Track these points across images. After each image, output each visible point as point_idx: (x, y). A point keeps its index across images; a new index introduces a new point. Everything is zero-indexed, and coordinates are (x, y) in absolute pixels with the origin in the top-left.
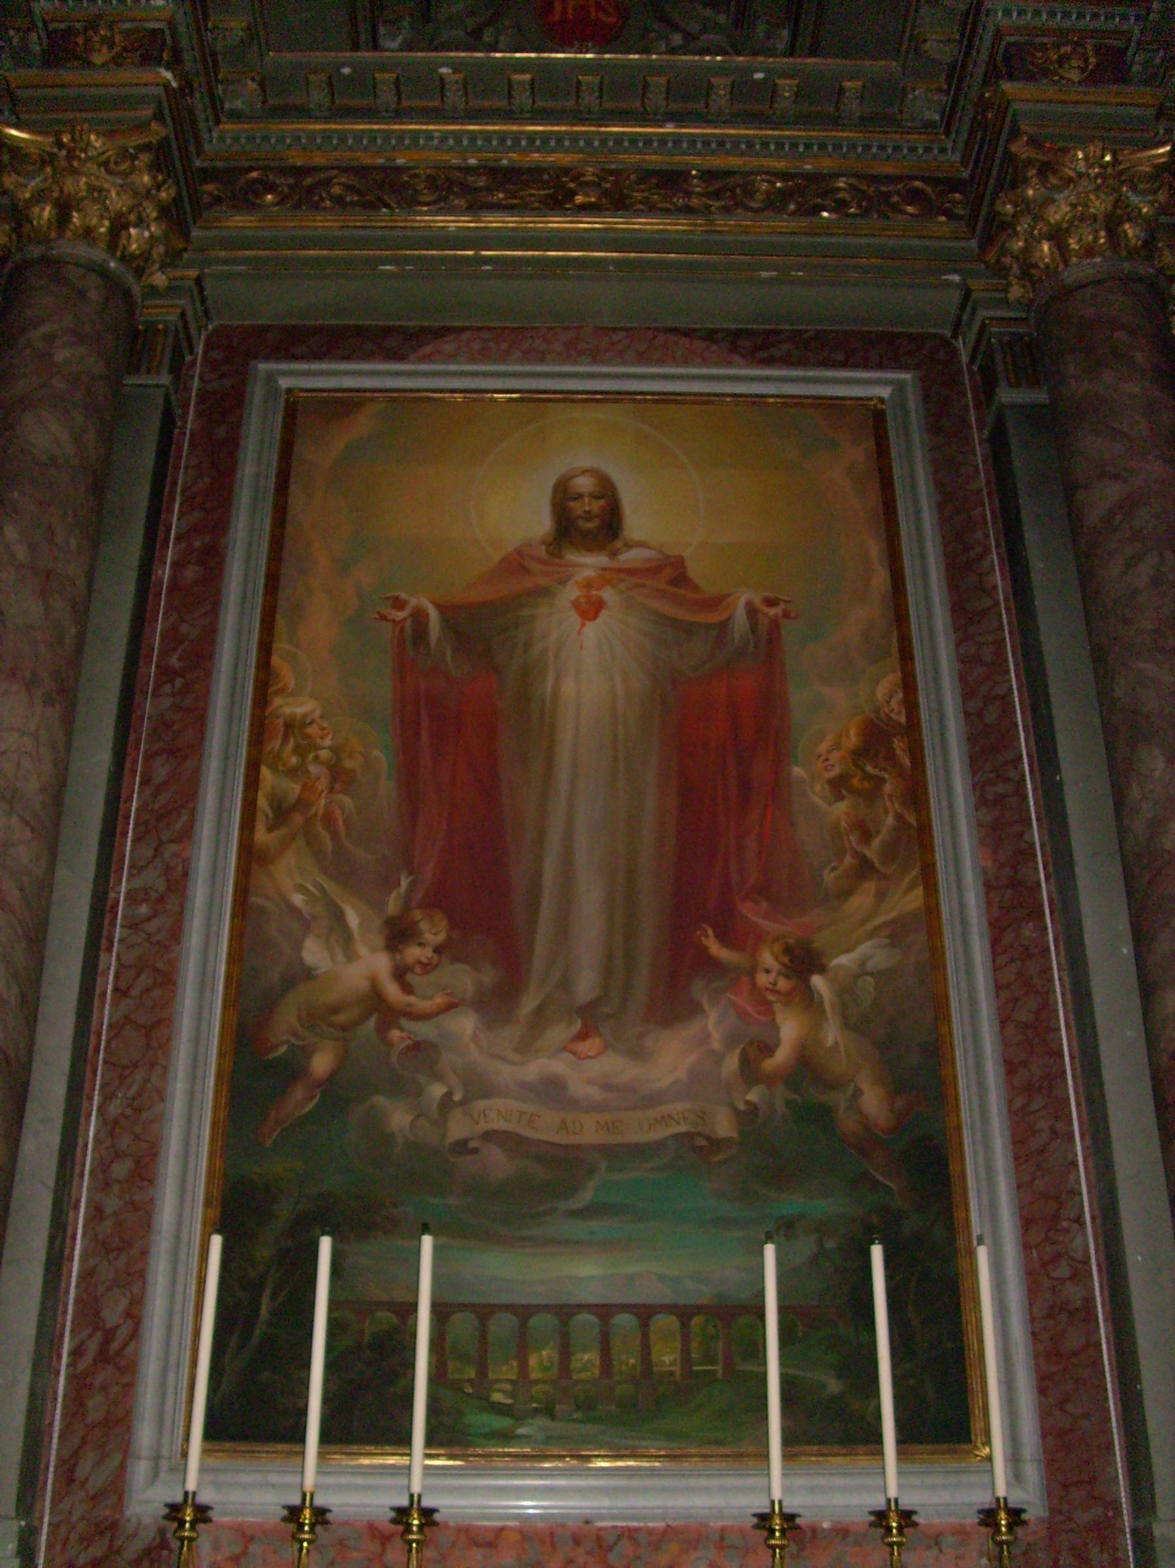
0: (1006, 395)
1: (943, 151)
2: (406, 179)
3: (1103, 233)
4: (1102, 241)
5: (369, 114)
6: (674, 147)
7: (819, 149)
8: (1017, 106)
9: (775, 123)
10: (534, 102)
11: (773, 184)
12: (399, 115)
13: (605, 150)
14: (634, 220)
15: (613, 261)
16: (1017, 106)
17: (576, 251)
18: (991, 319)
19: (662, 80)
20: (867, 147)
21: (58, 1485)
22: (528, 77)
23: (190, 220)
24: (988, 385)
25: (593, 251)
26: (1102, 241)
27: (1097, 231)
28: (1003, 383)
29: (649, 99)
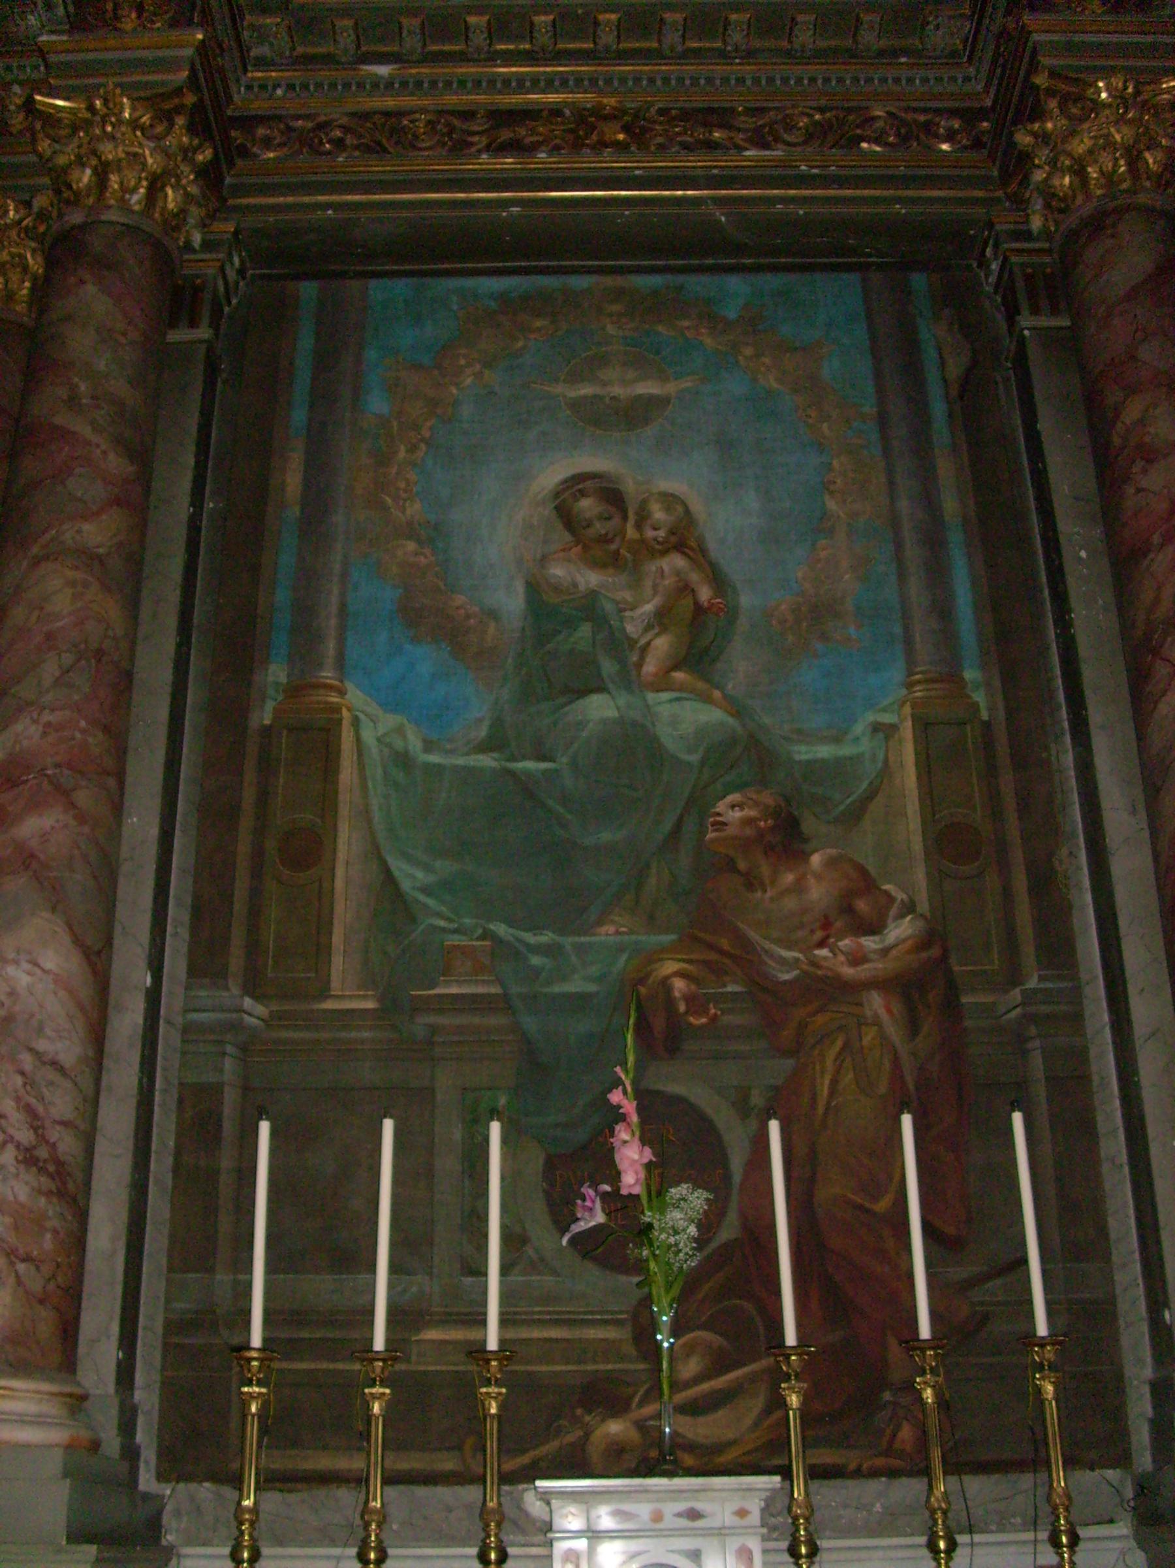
0: (1027, 322)
1: (967, 79)
2: (406, 122)
3: (1122, 162)
4: (1122, 169)
5: (463, 58)
6: (809, 85)
7: (634, 83)
8: (1035, 37)
9: (599, 58)
10: (425, 45)
11: (810, 116)
12: (492, 58)
13: (252, 97)
14: (502, 160)
15: (709, 198)
16: (1035, 37)
17: (600, 191)
18: (1013, 250)
19: (679, 17)
20: (827, 80)
21: (137, 1176)
22: (614, 17)
23: (225, 170)
24: (1012, 311)
25: (551, 191)
26: (1122, 169)
27: (1116, 160)
28: (1025, 312)
29: (797, 37)
